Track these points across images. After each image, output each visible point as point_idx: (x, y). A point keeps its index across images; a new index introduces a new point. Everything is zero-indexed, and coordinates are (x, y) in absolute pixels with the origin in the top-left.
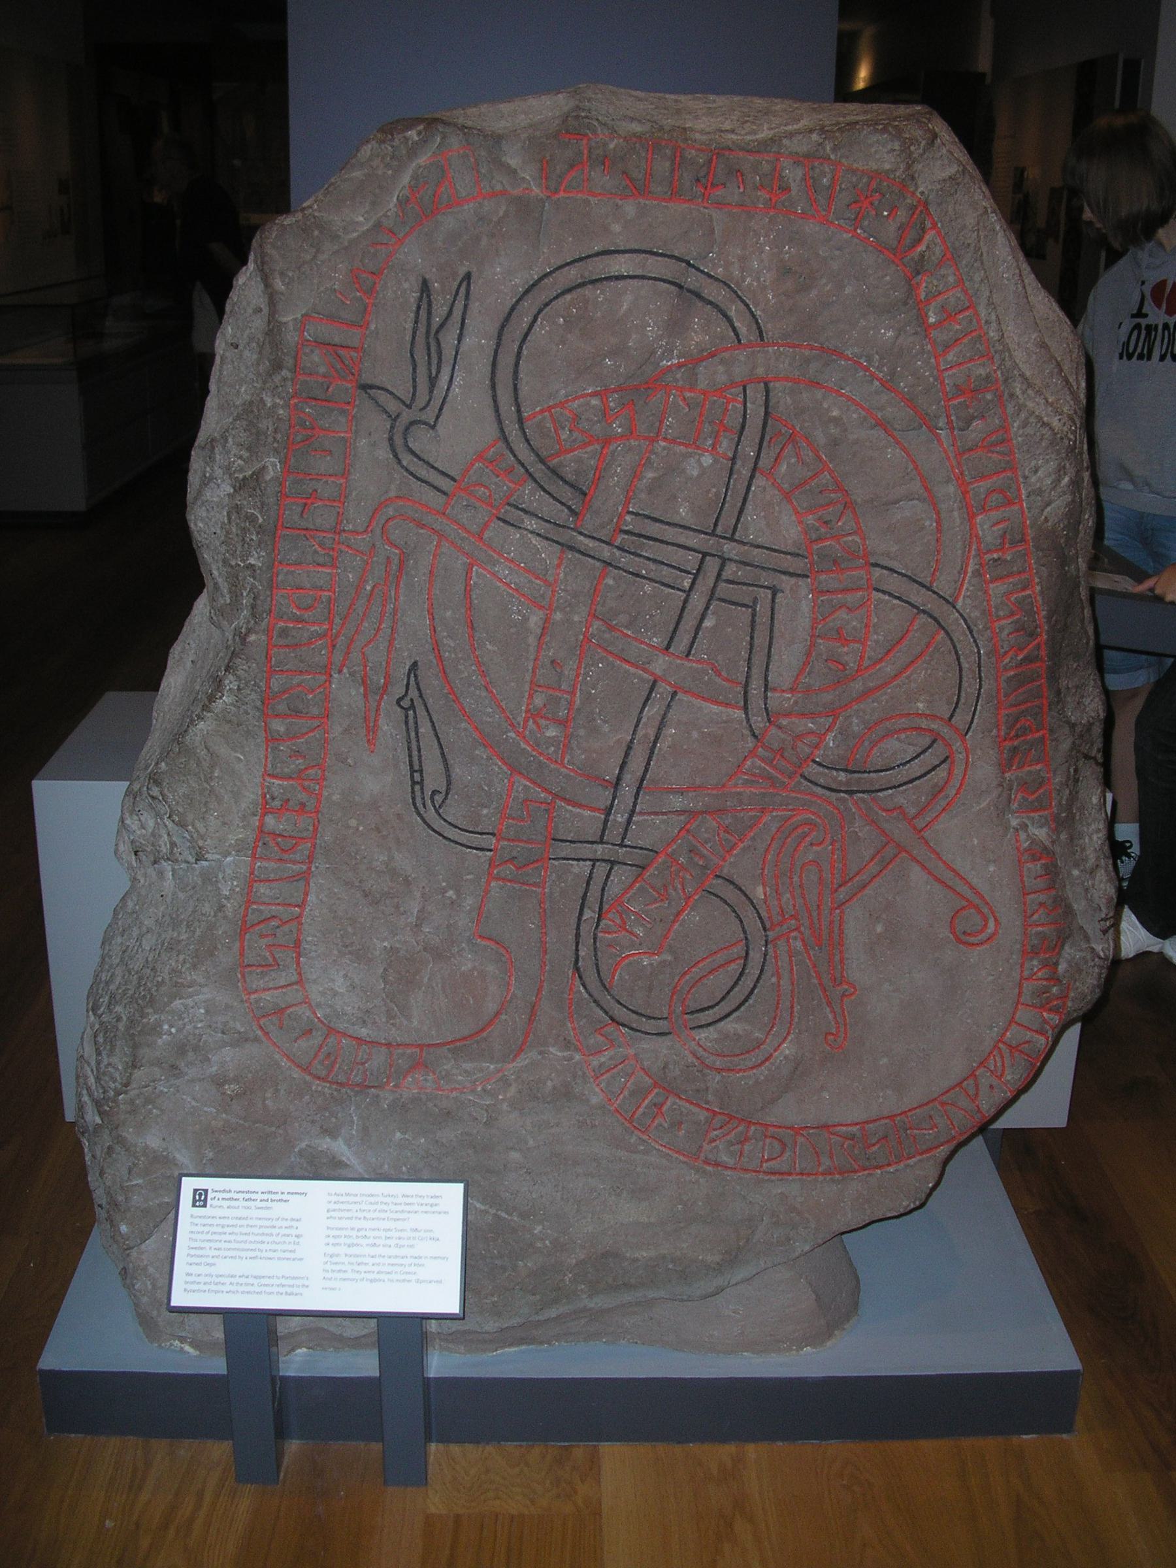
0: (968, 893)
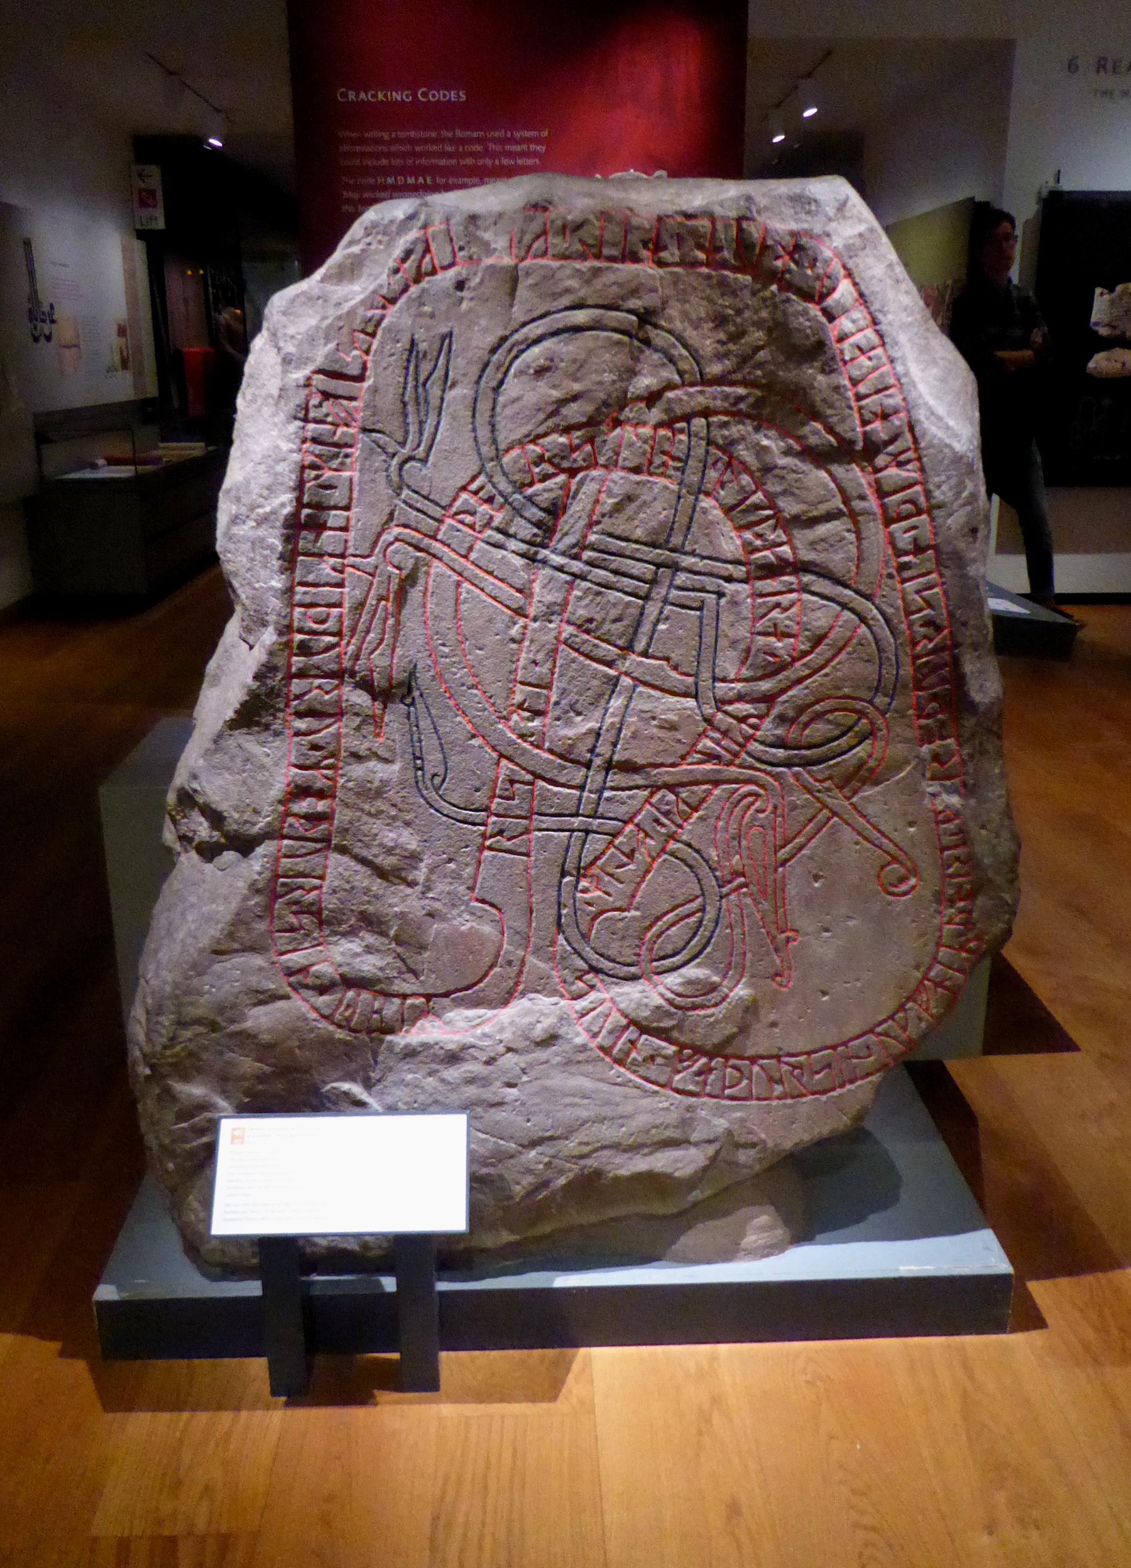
0: (890, 847)
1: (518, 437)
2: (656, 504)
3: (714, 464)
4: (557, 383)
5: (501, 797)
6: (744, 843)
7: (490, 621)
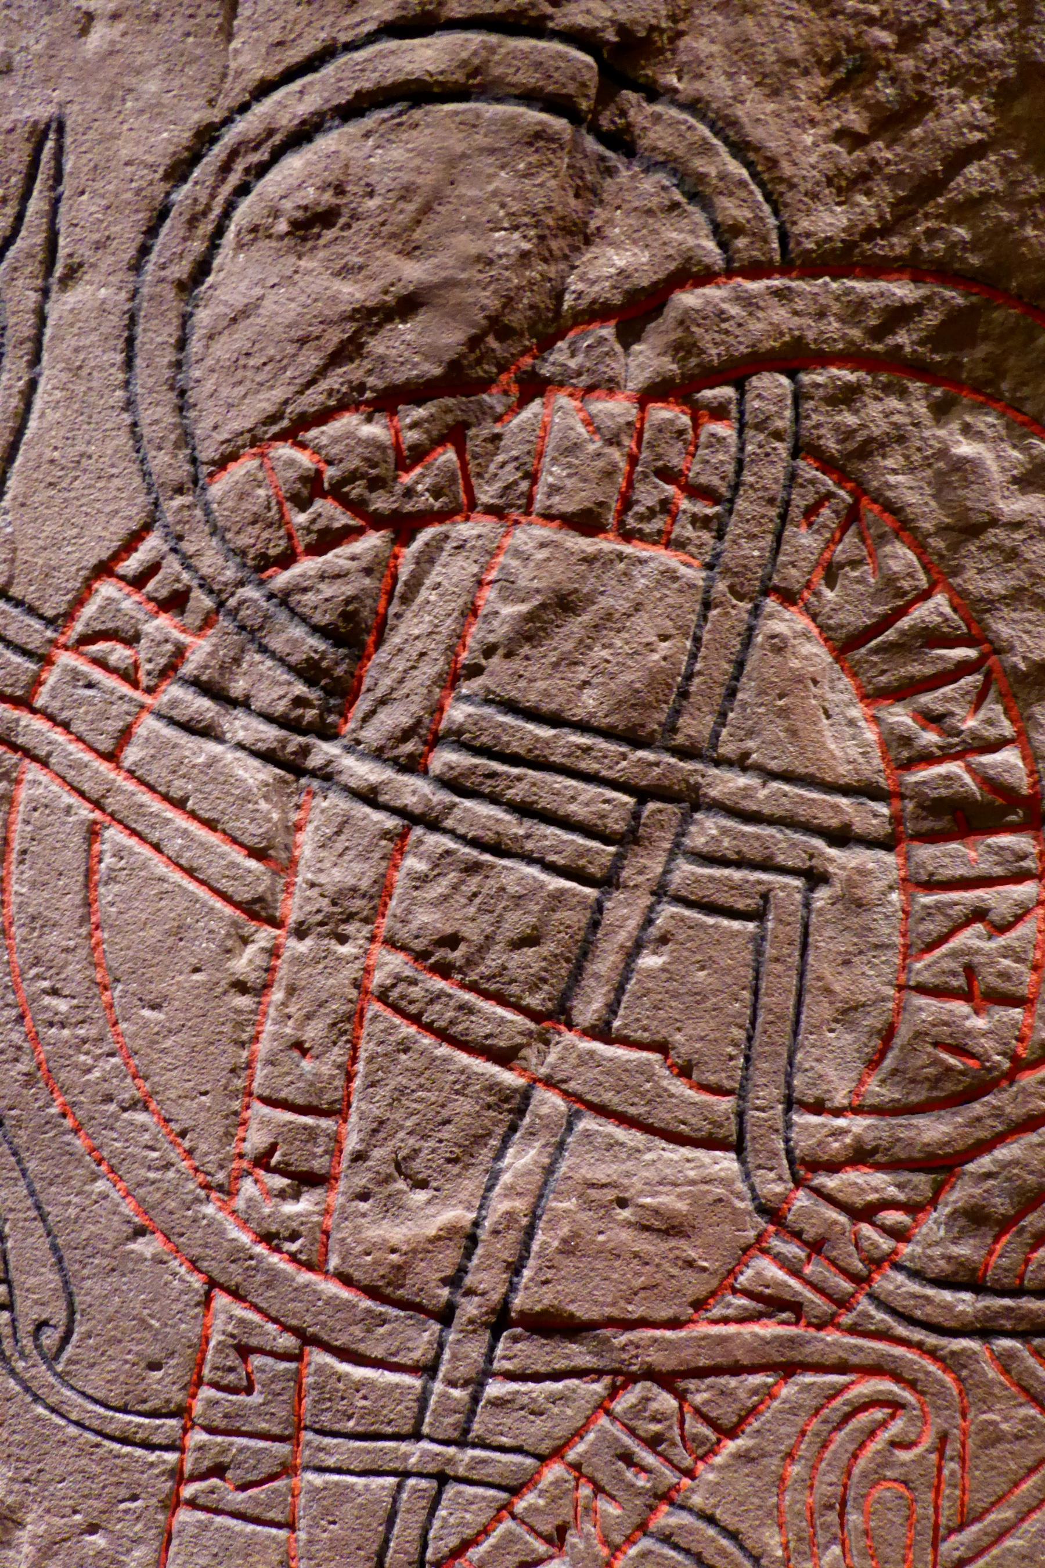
1: (249, 425)
2: (640, 621)
3: (811, 512)
4: (355, 259)
5: (215, 1385)
6: (854, 1518)
7: (179, 932)
